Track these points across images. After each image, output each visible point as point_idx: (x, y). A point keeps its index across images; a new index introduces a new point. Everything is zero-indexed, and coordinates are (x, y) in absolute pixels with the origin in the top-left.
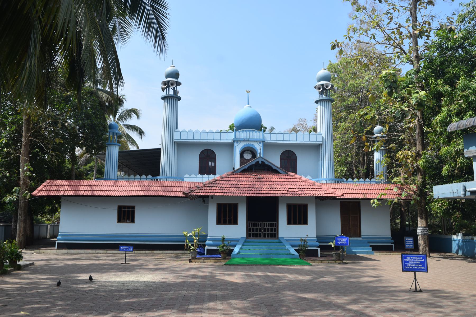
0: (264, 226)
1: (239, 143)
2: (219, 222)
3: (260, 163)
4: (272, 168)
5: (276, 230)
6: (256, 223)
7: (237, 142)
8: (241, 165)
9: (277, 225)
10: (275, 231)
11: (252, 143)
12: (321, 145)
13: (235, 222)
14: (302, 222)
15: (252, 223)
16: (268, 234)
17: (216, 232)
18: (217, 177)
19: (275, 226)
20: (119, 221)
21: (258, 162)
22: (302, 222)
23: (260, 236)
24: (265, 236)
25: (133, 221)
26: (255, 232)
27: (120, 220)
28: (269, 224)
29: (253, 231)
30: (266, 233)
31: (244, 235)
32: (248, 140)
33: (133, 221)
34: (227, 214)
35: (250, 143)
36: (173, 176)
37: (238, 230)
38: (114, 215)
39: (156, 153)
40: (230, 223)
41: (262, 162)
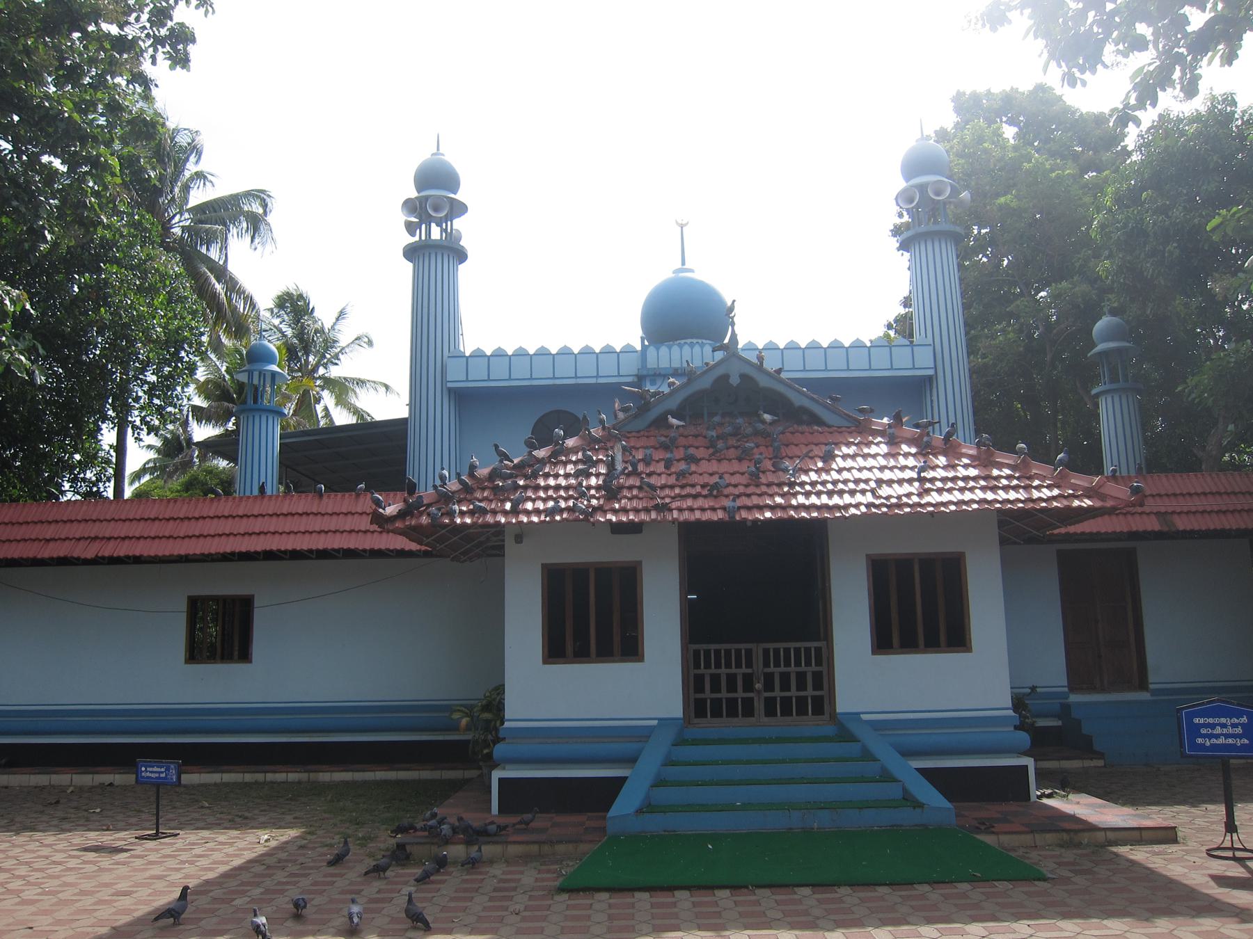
0: (766, 664)
3: (735, 381)
5: (824, 680)
6: (808, 650)
9: (824, 658)
10: (818, 685)
12: (930, 379)
13: (631, 649)
14: (236, 653)
15: (738, 652)
16: (802, 702)
17: (547, 695)
19: (819, 663)
20: (193, 656)
21: (725, 377)
23: (749, 711)
24: (770, 712)
25: (245, 656)
26: (724, 694)
27: (196, 652)
28: (787, 651)
29: (716, 688)
30: (777, 693)
31: (673, 706)
33: (245, 656)
34: (590, 618)
37: (645, 688)
38: (174, 632)
39: (394, 432)
40: (605, 653)
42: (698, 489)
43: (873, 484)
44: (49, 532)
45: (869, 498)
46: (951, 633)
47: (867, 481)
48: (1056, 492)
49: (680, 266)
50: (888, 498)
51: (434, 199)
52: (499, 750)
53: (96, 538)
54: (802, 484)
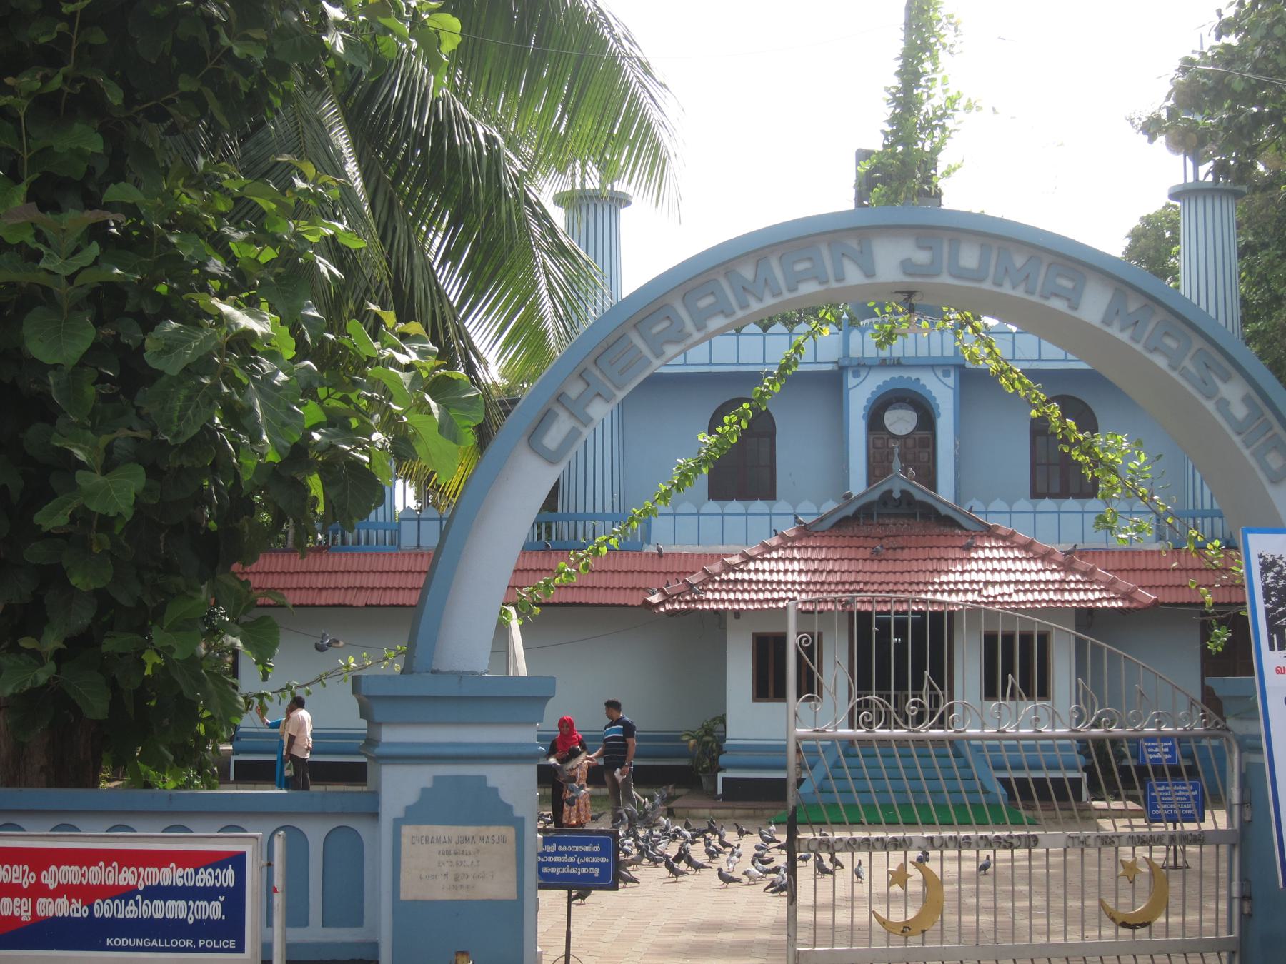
1: (863, 374)
3: (897, 495)
4: (936, 511)
7: (856, 375)
8: (869, 484)
11: (913, 375)
14: (771, 693)
18: (365, 789)
21: (890, 492)
22: (771, 693)
32: (897, 364)
35: (906, 374)
36: (608, 510)
41: (903, 492)
42: (862, 586)
43: (981, 585)
44: (320, 581)
45: (975, 597)
46: (1036, 684)
47: (978, 582)
48: (1104, 595)
50: (988, 597)
52: (723, 759)
53: (361, 588)
54: (933, 583)
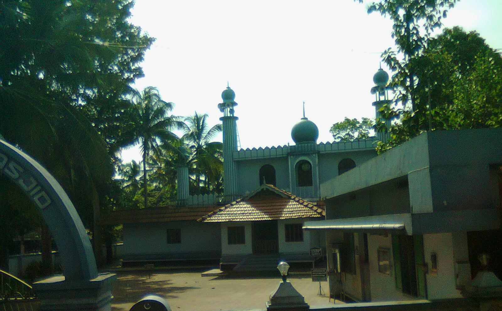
2: (230, 242)
3: (265, 189)
27: (169, 242)
49: (303, 117)
51: (228, 98)
